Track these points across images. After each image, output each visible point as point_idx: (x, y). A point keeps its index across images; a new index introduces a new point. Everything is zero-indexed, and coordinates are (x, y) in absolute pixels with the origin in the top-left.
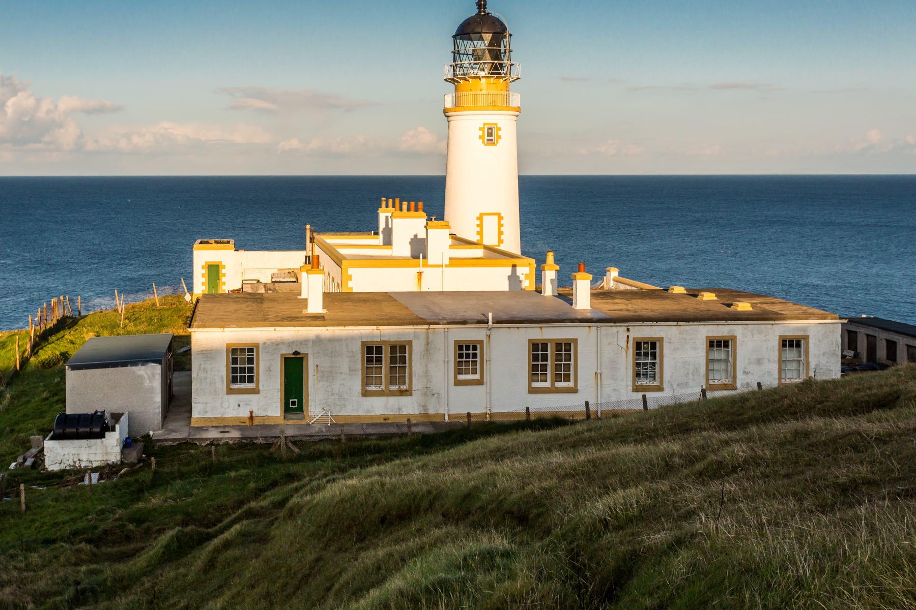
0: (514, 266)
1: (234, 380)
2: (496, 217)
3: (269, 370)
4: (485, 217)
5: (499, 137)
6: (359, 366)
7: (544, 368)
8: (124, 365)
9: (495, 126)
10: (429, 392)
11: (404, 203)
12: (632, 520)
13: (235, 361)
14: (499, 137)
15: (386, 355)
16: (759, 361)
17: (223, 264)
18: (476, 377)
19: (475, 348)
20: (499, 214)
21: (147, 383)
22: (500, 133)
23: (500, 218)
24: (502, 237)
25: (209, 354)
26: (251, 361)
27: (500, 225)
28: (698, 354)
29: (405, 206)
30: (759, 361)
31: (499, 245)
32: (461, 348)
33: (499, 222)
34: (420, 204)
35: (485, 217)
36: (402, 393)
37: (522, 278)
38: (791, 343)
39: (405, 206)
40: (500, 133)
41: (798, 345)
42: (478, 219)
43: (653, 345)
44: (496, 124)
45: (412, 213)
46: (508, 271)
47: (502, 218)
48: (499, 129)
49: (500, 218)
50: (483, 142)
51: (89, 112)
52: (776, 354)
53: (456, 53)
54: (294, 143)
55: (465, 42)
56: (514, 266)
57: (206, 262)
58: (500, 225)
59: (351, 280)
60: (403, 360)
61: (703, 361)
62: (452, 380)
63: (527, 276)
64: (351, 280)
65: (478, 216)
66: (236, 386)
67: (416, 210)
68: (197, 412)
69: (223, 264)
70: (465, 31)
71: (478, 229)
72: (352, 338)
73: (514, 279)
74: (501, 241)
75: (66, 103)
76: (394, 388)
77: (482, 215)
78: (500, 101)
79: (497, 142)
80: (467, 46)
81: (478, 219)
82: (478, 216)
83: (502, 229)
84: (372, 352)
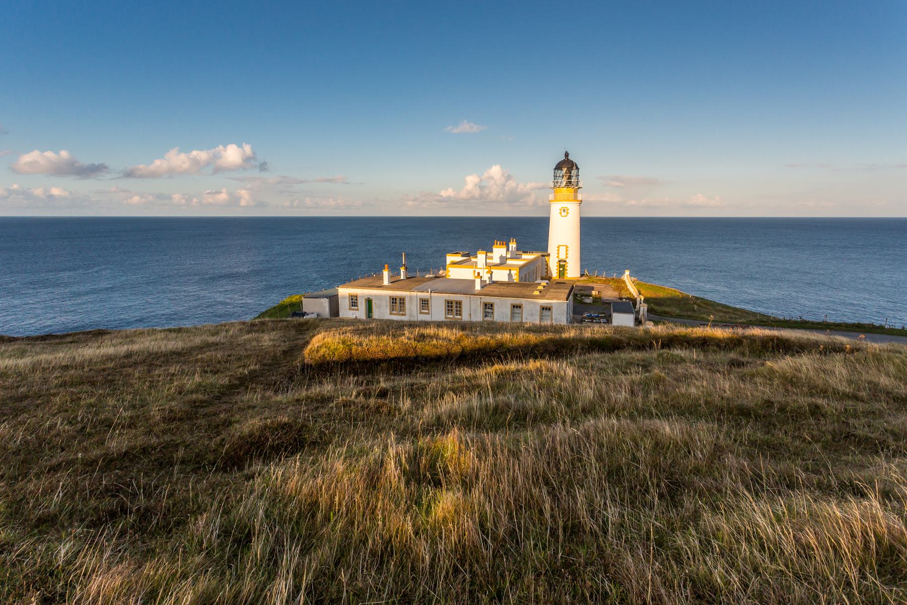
0: (510, 270)
1: (352, 306)
3: (361, 303)
6: (389, 304)
7: (452, 310)
8: (315, 298)
10: (411, 315)
12: (677, 382)
13: (352, 299)
15: (398, 301)
16: (532, 315)
18: (427, 311)
19: (427, 301)
21: (324, 304)
23: (567, 247)
25: (344, 297)
26: (356, 300)
27: (558, 253)
28: (508, 311)
29: (498, 244)
30: (532, 315)
32: (448, 303)
34: (504, 243)
35: (561, 247)
36: (402, 315)
37: (513, 275)
38: (546, 309)
39: (498, 244)
41: (550, 309)
43: (492, 305)
45: (501, 246)
46: (508, 272)
49: (567, 247)
51: (539, 189)
52: (538, 313)
53: (555, 176)
54: (634, 202)
56: (510, 270)
58: (567, 251)
60: (404, 303)
61: (509, 313)
62: (419, 312)
63: (515, 274)
66: (352, 308)
67: (503, 245)
68: (341, 315)
70: (559, 167)
72: (385, 296)
73: (510, 275)
74: (567, 257)
75: (529, 186)
76: (401, 313)
77: (559, 246)
78: (573, 197)
80: (559, 173)
84: (393, 300)
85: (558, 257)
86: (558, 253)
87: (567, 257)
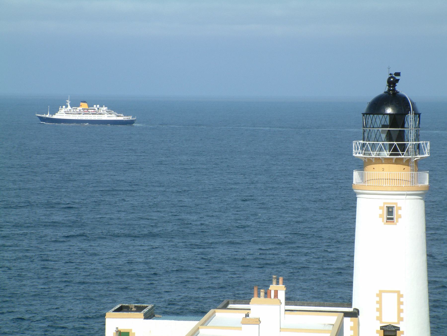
2: (396, 295)
4: (383, 294)
5: (400, 216)
9: (395, 206)
11: (262, 290)
14: (400, 216)
17: (133, 332)
20: (398, 292)
22: (400, 212)
23: (400, 296)
24: (402, 315)
27: (379, 310)
31: (398, 323)
33: (399, 300)
35: (384, 295)
40: (400, 212)
42: (378, 295)
44: (396, 204)
47: (402, 296)
48: (400, 208)
49: (400, 296)
50: (383, 221)
55: (376, 116)
57: (396, 224)
58: (400, 303)
59: (377, 317)
64: (377, 317)
65: (378, 293)
69: (133, 332)
71: (402, 300)
79: (397, 221)
81: (378, 295)
82: (378, 293)
83: (402, 307)
85: (379, 318)
86: (379, 310)
87: (401, 319)
